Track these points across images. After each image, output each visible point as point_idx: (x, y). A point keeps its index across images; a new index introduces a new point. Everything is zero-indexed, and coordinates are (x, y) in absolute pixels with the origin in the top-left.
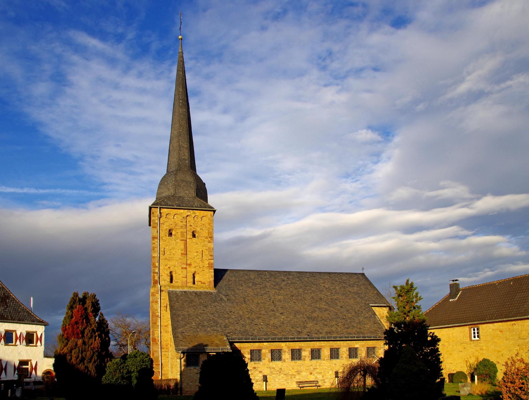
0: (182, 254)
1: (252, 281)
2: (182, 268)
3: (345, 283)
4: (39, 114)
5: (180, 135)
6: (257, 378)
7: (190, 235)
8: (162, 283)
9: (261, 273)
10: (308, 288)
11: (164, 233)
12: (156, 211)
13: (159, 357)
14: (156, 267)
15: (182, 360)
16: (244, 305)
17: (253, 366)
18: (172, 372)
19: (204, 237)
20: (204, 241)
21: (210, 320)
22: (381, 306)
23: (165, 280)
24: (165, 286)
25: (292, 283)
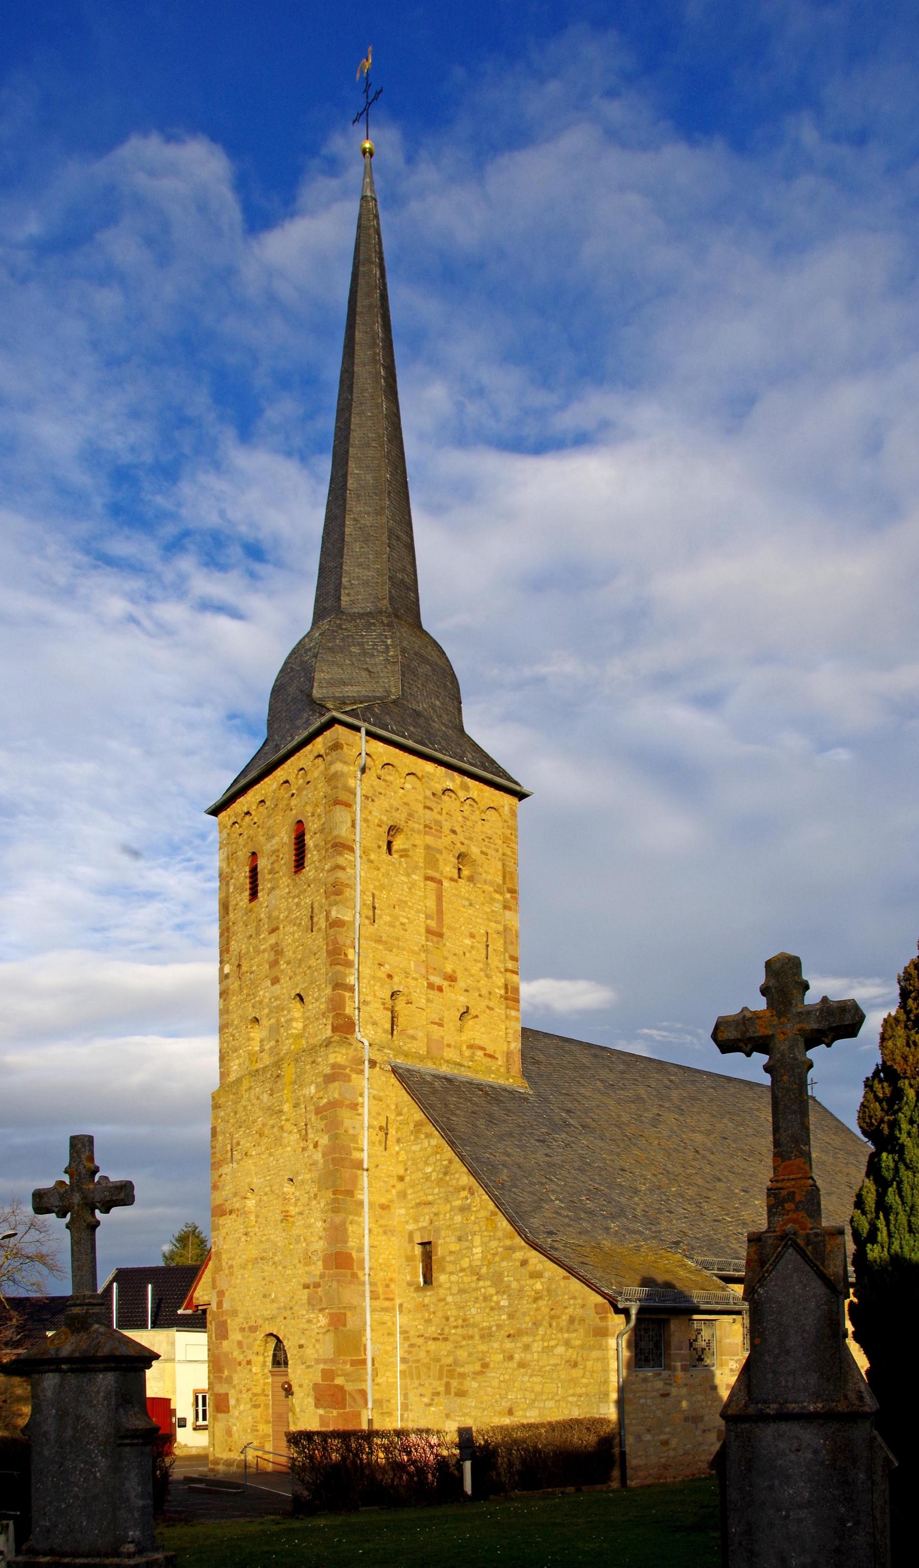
0: (429, 931)
19: (491, 883)
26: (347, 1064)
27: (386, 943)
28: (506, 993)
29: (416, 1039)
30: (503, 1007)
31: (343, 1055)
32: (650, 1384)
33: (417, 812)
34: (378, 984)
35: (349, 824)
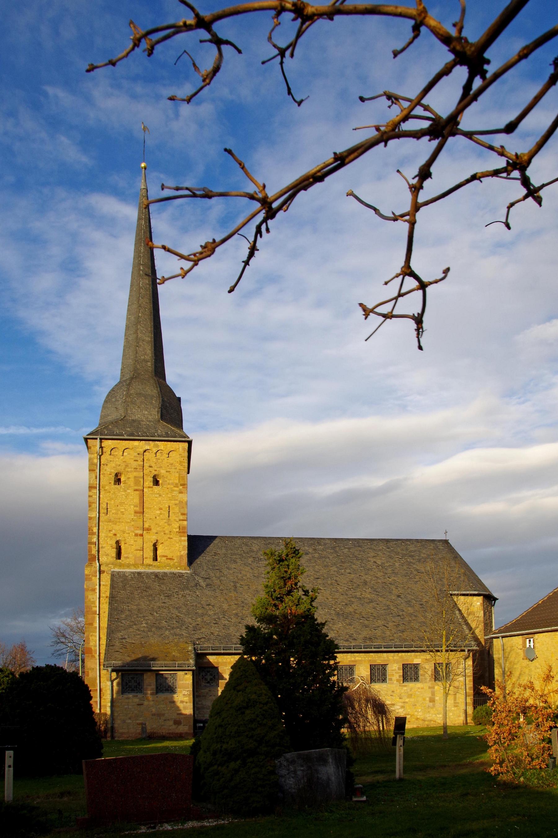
0: (136, 512)
1: (253, 555)
2: (136, 535)
3: (412, 556)
4: (36, 319)
5: (138, 322)
7: (149, 482)
8: (103, 559)
9: (271, 541)
10: (346, 565)
13: (96, 679)
14: (93, 534)
15: (115, 683)
16: (233, 594)
19: (172, 484)
20: (173, 491)
21: (172, 618)
22: (467, 595)
23: (107, 555)
24: (107, 565)
25: (320, 557)
27: (113, 521)
29: (129, 558)
32: (130, 700)
35: (94, 478)
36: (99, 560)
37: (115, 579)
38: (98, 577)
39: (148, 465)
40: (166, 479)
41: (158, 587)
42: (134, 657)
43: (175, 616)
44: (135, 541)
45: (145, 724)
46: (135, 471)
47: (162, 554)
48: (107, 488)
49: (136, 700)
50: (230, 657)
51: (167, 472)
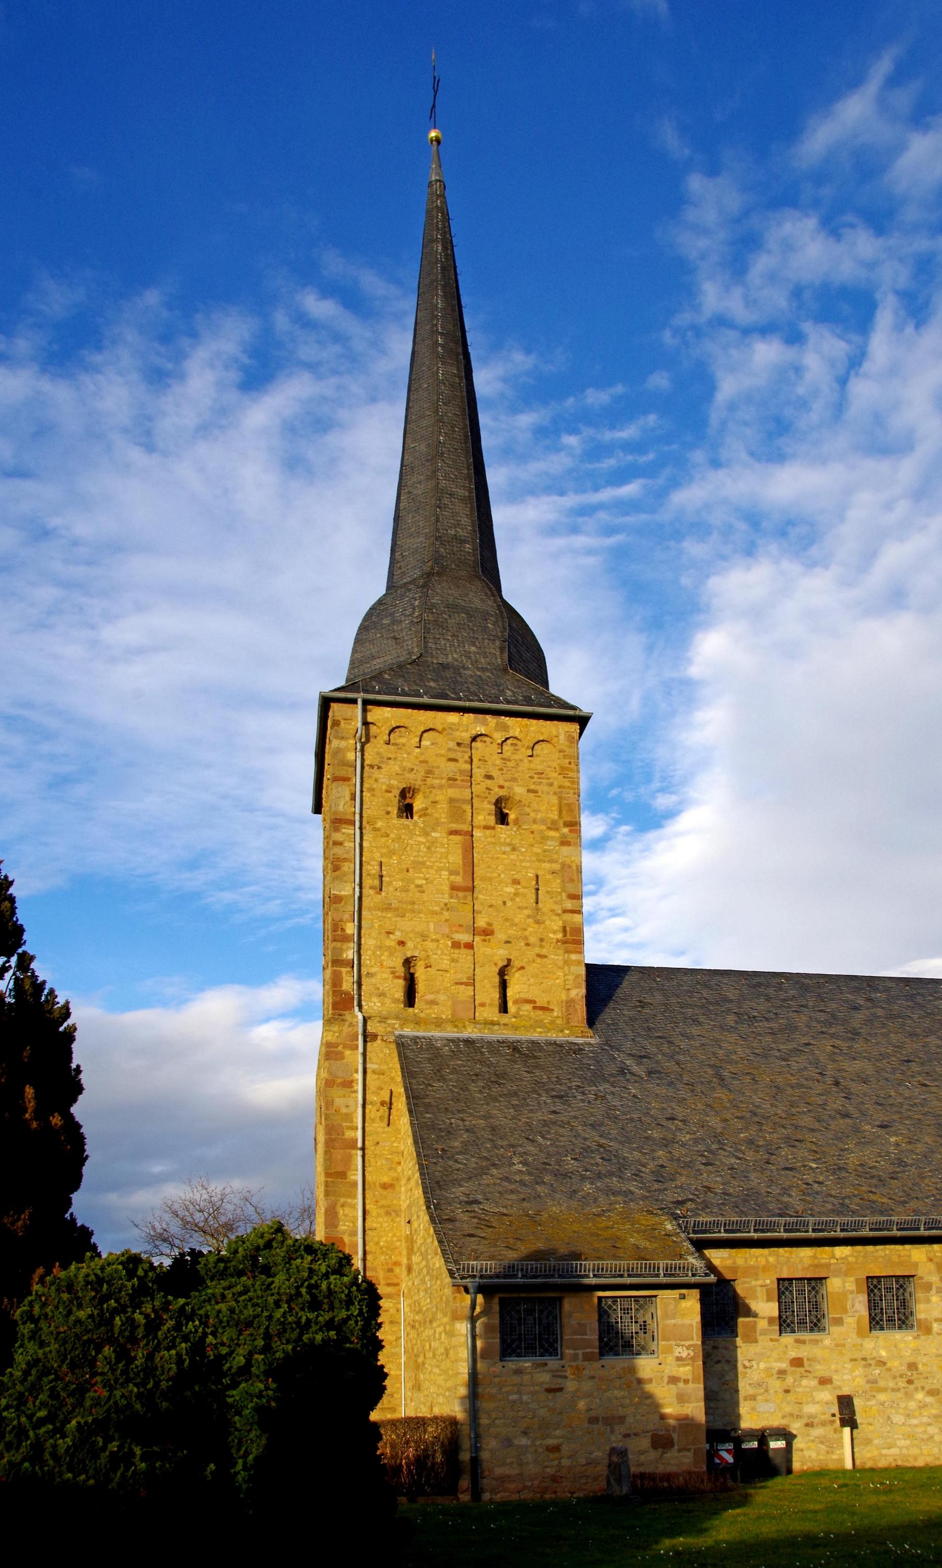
0: (454, 888)
2: (456, 945)
6: (810, 1409)
7: (485, 815)
8: (372, 1005)
9: (761, 980)
11: (380, 804)
12: (349, 717)
14: (346, 939)
15: (478, 1324)
16: (720, 1094)
17: (793, 1354)
18: (417, 1387)
19: (543, 821)
20: (545, 838)
21: (587, 1149)
23: (382, 995)
24: (383, 1019)
25: (891, 1017)
26: (339, 1041)
27: (397, 909)
28: (565, 935)
29: (437, 1004)
30: (561, 952)
31: (335, 1032)
32: (526, 1378)
33: (438, 767)
34: (386, 953)
35: (348, 797)
36: (360, 1006)
37: (410, 1055)
38: (361, 1049)
39: (483, 772)
40: (527, 809)
41: (525, 1074)
42: (524, 1249)
43: (593, 1146)
44: (453, 960)
45: (613, 1449)
46: (450, 786)
47: (523, 996)
48: (379, 824)
49: (544, 1378)
50: (766, 1251)
51: (529, 791)
